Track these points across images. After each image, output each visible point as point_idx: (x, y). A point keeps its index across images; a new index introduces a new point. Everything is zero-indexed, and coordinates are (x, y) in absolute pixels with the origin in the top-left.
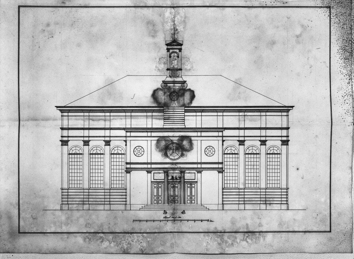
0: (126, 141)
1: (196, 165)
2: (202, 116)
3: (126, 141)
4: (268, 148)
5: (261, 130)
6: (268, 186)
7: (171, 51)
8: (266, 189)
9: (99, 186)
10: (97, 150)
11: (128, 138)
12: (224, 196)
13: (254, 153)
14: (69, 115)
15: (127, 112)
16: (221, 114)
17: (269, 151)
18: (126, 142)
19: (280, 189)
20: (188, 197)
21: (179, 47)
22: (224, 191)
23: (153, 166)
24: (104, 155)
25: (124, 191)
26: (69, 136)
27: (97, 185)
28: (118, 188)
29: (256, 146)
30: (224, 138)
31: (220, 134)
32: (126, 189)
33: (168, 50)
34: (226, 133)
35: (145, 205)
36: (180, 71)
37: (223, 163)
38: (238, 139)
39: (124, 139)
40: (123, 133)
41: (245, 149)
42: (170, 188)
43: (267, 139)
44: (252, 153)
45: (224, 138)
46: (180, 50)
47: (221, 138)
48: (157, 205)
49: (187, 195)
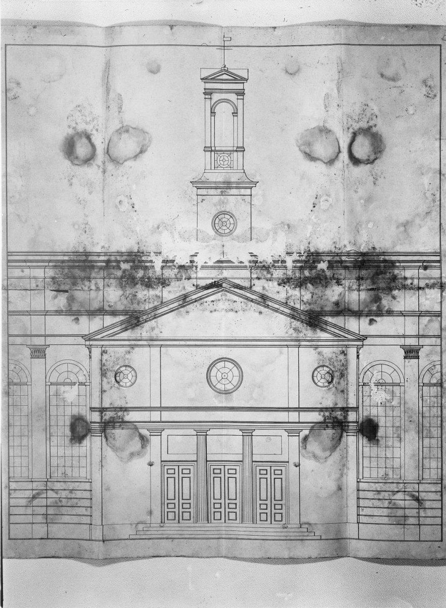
1: (147, 413)
4: (53, 368)
6: (366, 474)
7: (216, 97)
8: (420, 483)
10: (231, 372)
17: (55, 374)
19: (87, 482)
20: (276, 506)
21: (240, 86)
23: (166, 416)
24: (402, 388)
29: (390, 364)
33: (208, 93)
36: (240, 154)
37: (358, 408)
38: (401, 341)
41: (47, 371)
42: (258, 478)
43: (47, 343)
44: (68, 381)
46: (241, 93)
49: (258, 499)
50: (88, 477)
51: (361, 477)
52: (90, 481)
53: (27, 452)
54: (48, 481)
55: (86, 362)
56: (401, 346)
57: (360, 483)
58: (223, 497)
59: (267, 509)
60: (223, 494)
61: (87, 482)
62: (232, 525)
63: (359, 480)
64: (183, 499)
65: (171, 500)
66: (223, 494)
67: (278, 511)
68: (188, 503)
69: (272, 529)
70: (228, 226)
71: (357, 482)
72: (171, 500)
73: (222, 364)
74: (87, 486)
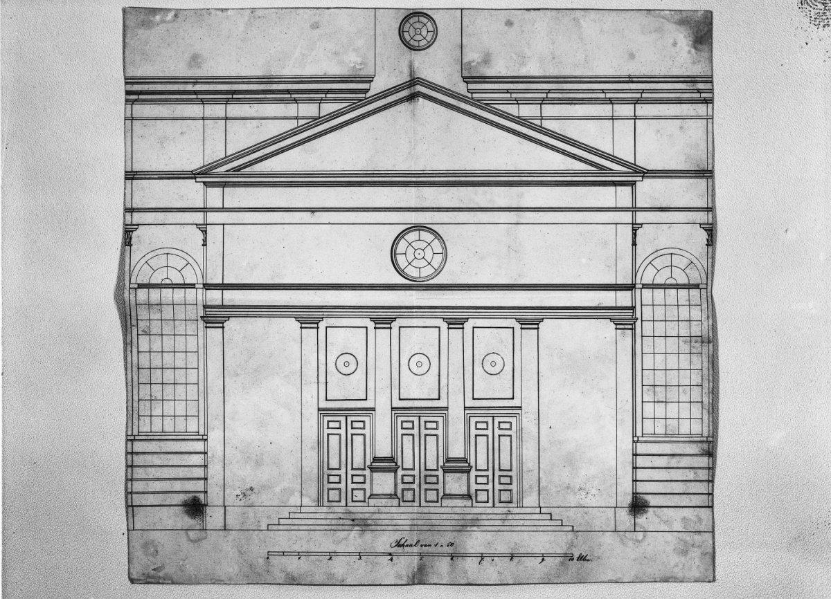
0: (203, 228)
2: (635, 118)
3: (203, 228)
5: (618, 188)
9: (181, 426)
11: (212, 217)
12: (641, 474)
13: (677, 285)
14: (615, 114)
15: (208, 100)
16: (218, 110)
18: (206, 231)
19: (198, 440)
22: (641, 448)
25: (199, 446)
26: (134, 206)
27: (180, 421)
28: (673, 435)
30: (641, 217)
31: (623, 196)
32: (206, 440)
34: (649, 190)
35: (293, 510)
39: (198, 218)
40: (192, 193)
41: (639, 262)
44: (168, 282)
45: (641, 217)
47: (627, 217)
48: (489, 511)
50: (202, 432)
51: (639, 434)
52: (205, 437)
53: (142, 407)
54: (135, 440)
55: (198, 253)
56: (700, 224)
57: (638, 444)
58: (423, 438)
59: (340, 483)
60: (423, 442)
61: (198, 440)
62: (432, 510)
63: (636, 439)
64: (352, 469)
65: (432, 490)
66: (423, 442)
67: (407, 486)
68: (435, 490)
69: (530, 521)
70: (415, 263)
71: (634, 441)
72: (432, 490)
73: (416, 19)
74: (199, 446)
